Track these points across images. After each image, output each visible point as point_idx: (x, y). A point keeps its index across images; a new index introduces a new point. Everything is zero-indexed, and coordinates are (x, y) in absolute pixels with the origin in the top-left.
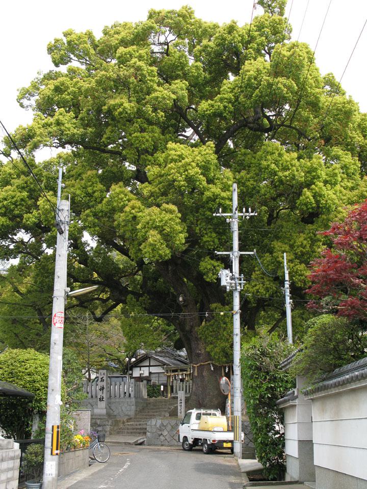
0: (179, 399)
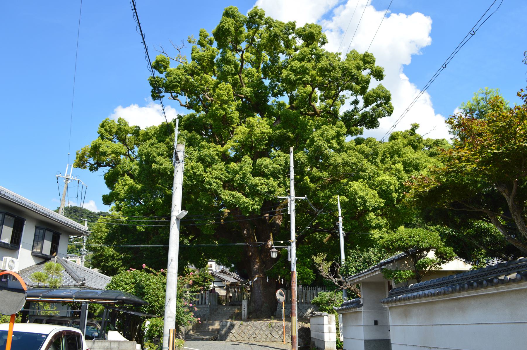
0: (243, 306)
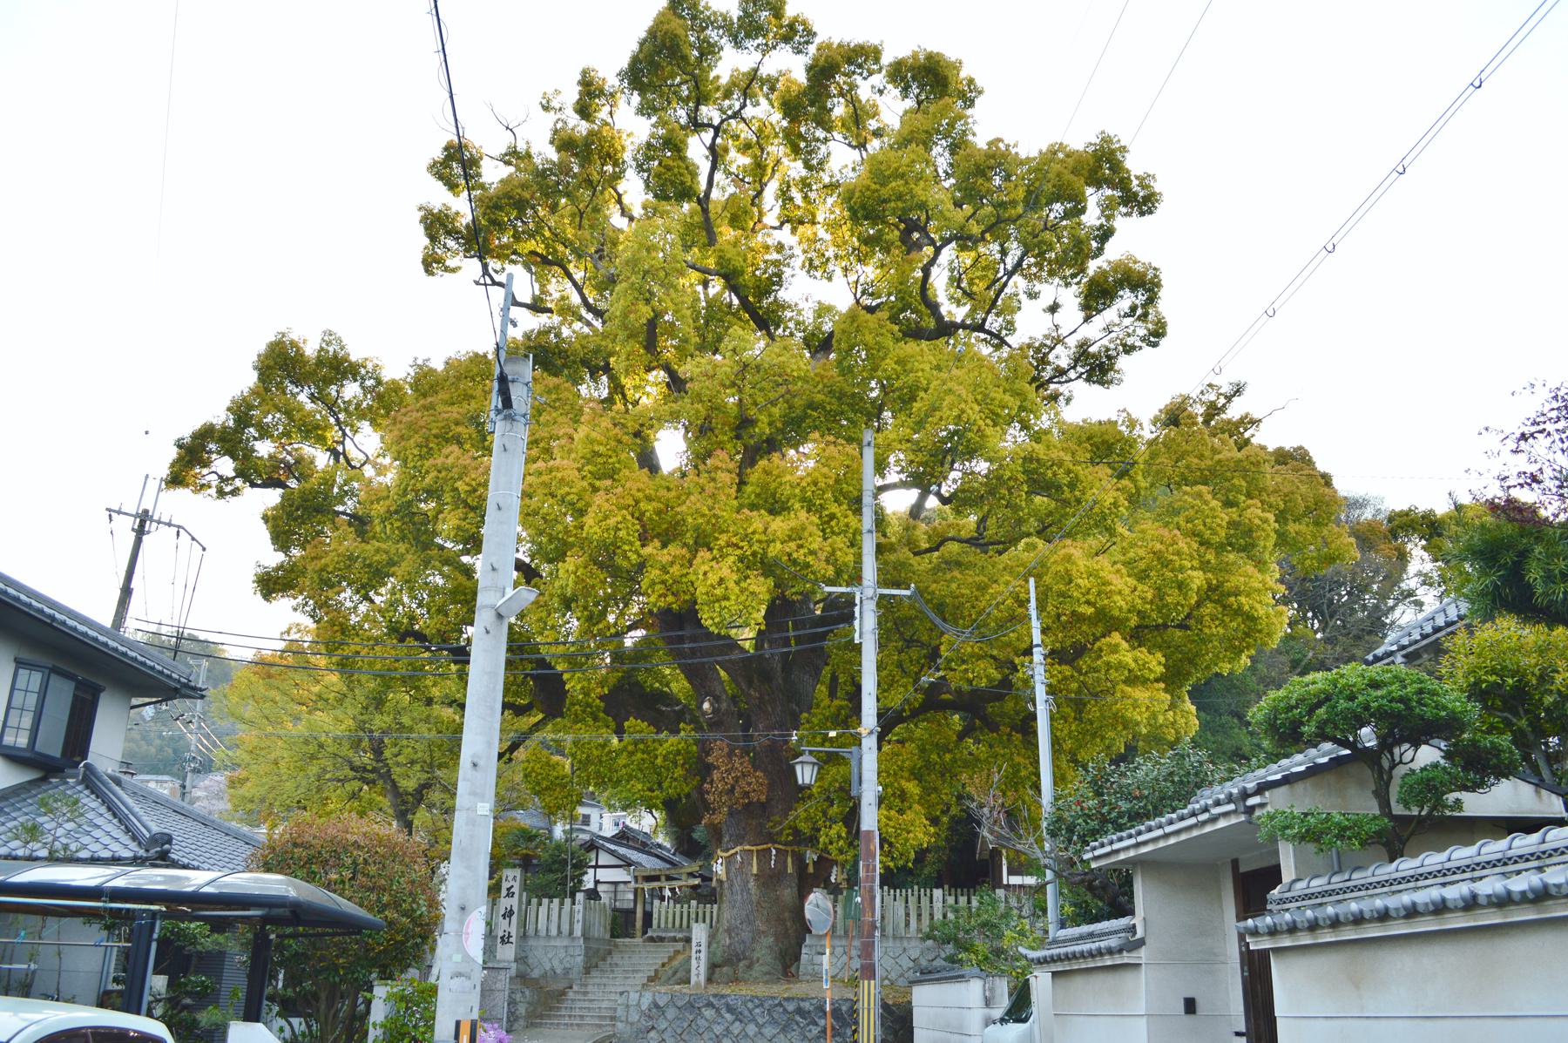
0: (694, 943)
